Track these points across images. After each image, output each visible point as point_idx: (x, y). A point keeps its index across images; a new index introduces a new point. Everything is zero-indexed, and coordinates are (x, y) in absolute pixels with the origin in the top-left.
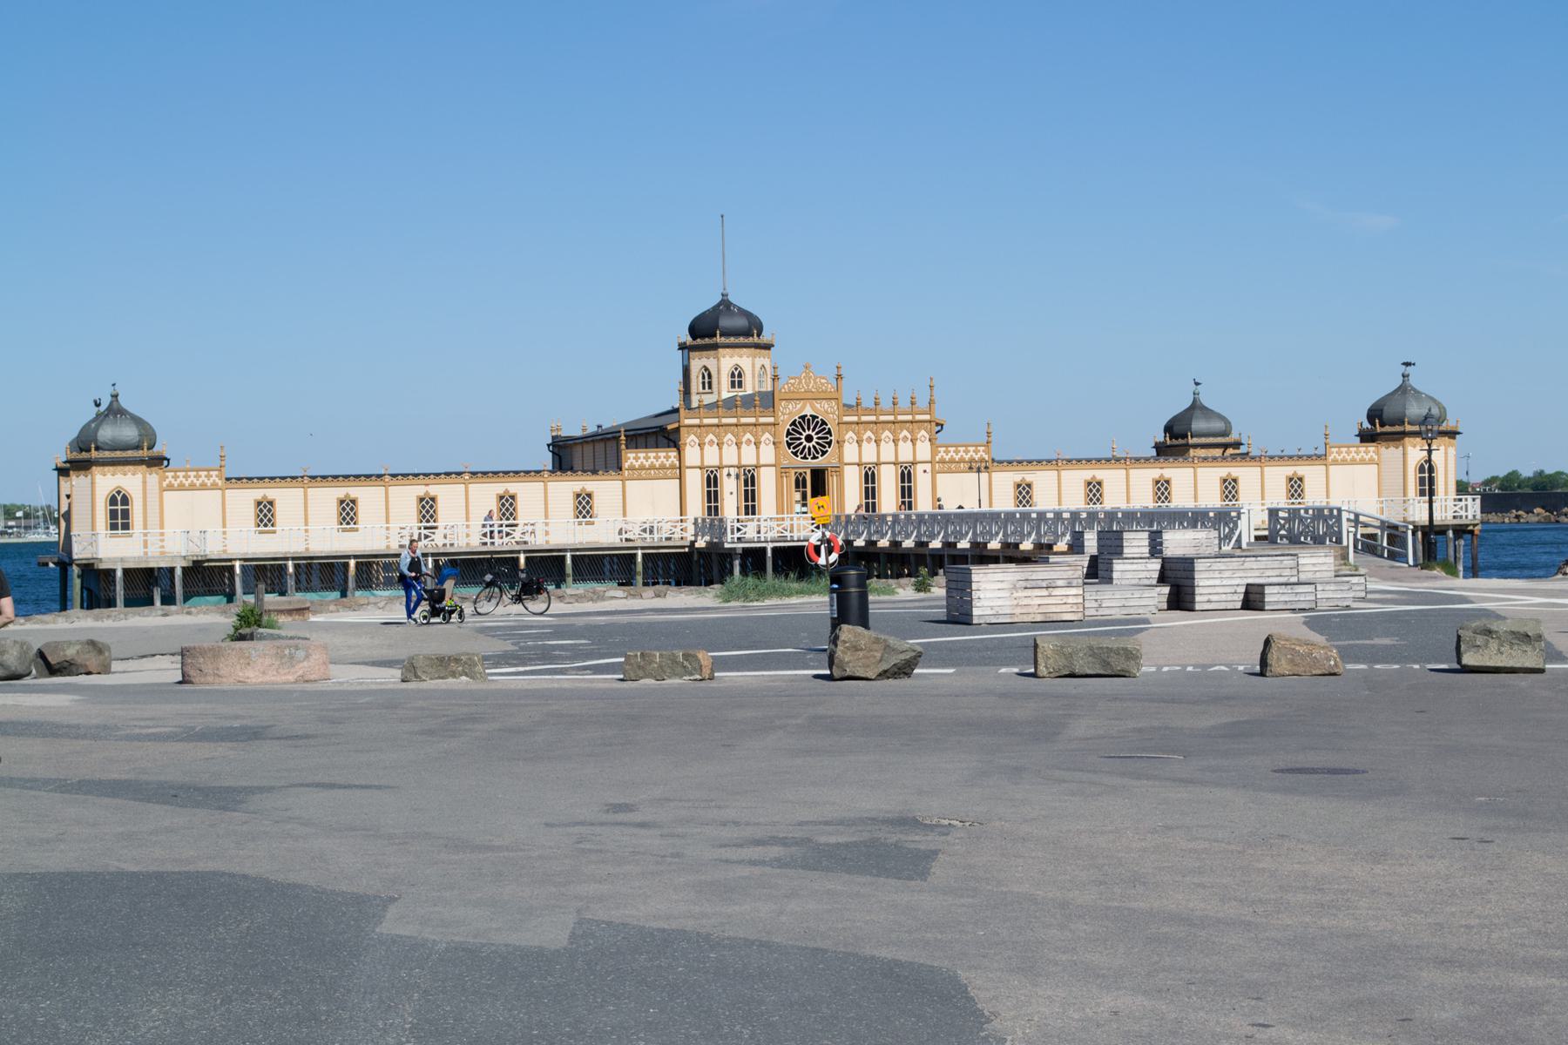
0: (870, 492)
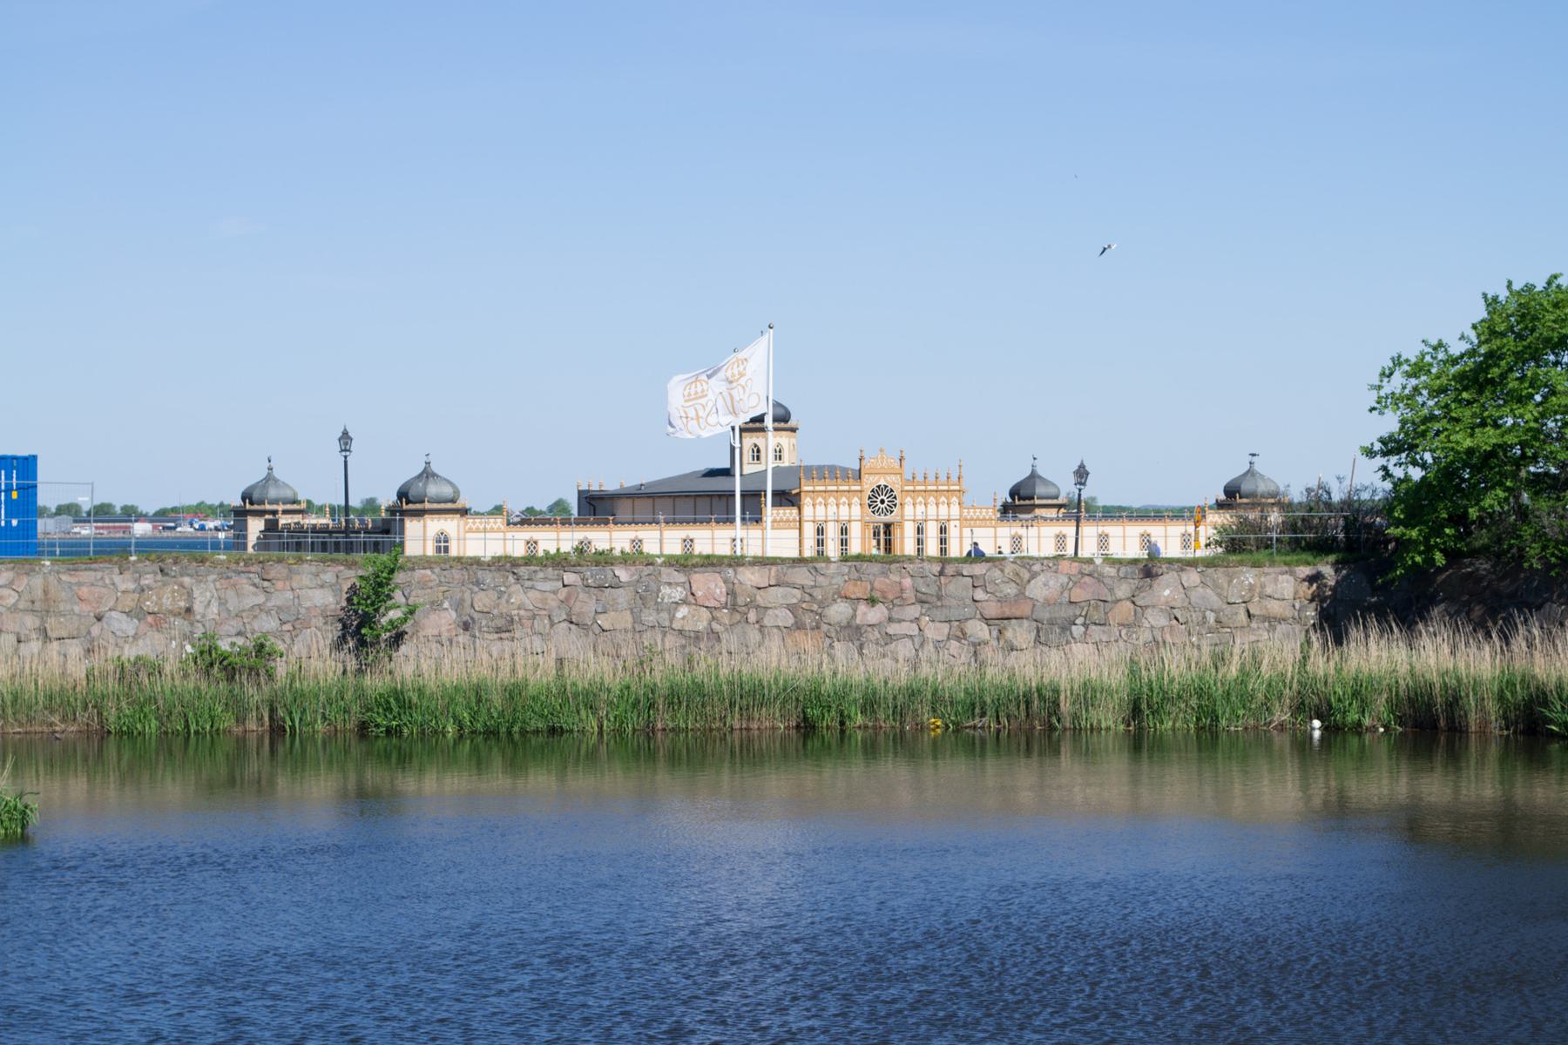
0: (820, 543)
